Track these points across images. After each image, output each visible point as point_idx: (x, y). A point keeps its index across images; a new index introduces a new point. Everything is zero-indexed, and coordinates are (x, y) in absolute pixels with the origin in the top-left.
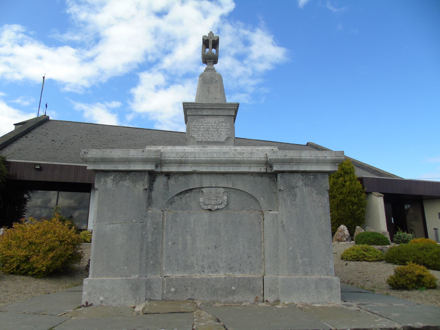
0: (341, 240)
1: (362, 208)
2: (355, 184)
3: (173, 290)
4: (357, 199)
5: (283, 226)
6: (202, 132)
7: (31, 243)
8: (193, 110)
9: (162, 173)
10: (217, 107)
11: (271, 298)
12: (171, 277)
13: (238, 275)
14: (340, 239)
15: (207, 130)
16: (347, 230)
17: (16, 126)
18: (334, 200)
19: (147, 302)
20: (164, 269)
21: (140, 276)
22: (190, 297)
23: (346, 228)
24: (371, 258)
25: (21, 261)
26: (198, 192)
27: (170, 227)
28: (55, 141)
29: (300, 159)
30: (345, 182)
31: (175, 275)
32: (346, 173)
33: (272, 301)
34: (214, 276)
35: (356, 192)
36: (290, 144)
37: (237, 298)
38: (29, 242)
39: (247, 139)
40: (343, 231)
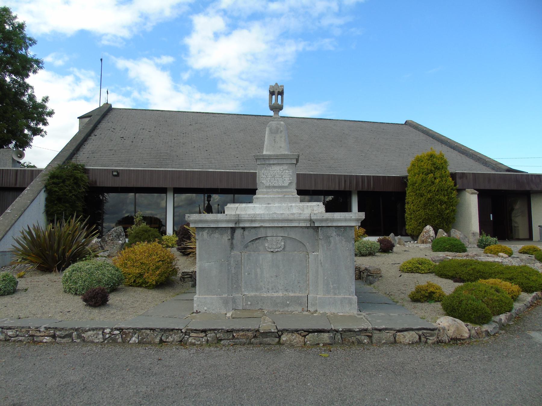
0: (426, 242)
1: (452, 207)
2: (446, 181)
3: (249, 303)
4: (447, 197)
5: (321, 263)
6: (270, 179)
7: (142, 263)
8: (262, 160)
9: (239, 227)
10: (281, 157)
11: (312, 309)
12: (248, 295)
13: (291, 294)
14: (424, 241)
15: (274, 177)
16: (433, 231)
17: (81, 119)
18: (422, 198)
19: (233, 311)
20: (243, 290)
21: (228, 295)
22: (260, 308)
23: (432, 229)
24: (423, 270)
25: (136, 276)
26: (265, 239)
27: (246, 263)
28: (124, 138)
29: (333, 219)
30: (435, 178)
31: (250, 294)
32: (437, 168)
33: (313, 311)
34: (276, 295)
35: (447, 190)
36: (385, 123)
37: (290, 309)
38: (141, 263)
39: (333, 120)
40: (428, 232)
